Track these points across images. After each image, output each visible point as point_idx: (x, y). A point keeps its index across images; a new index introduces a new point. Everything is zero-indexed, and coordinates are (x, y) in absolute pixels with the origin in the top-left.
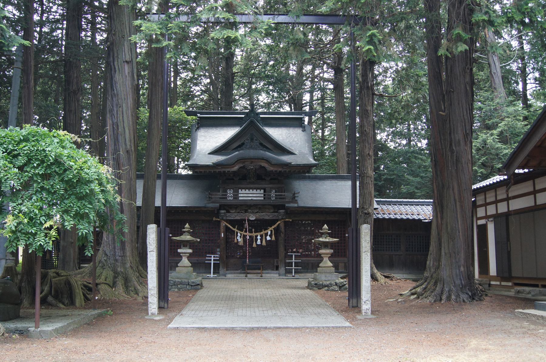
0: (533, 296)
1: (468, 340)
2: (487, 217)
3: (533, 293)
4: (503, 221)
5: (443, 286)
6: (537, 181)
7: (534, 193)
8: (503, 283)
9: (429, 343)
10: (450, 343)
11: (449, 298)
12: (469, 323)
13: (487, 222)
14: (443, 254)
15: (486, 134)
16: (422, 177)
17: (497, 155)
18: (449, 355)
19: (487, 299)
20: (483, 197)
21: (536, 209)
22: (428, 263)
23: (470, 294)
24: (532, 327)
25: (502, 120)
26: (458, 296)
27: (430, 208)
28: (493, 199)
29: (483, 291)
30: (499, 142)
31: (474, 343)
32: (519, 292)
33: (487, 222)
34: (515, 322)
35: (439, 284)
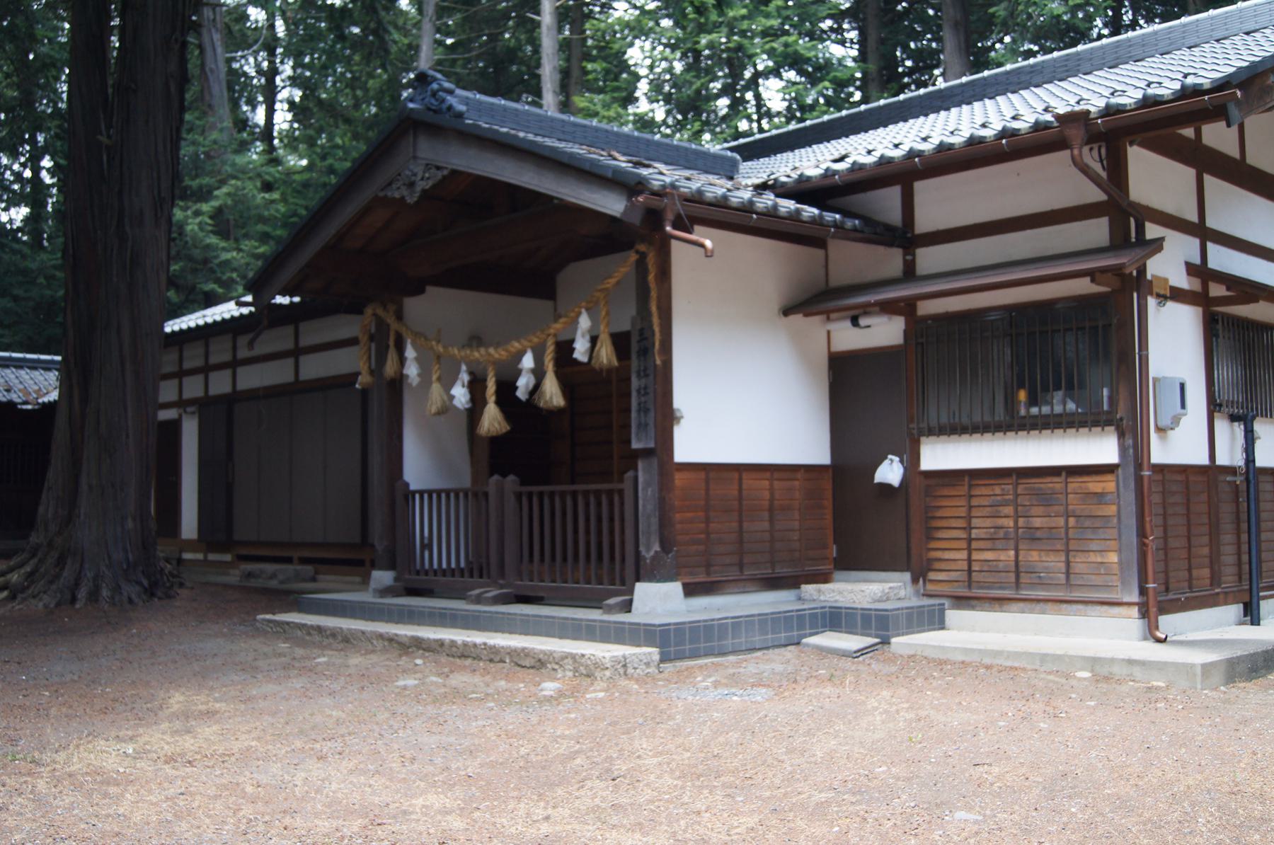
0: (282, 582)
1: (162, 694)
2: (181, 404)
3: (281, 577)
4: (220, 414)
5: (82, 565)
6: (304, 326)
7: (297, 353)
8: (211, 557)
9: (64, 710)
10: (117, 705)
11: (94, 596)
12: (154, 652)
13: (180, 416)
14: (84, 487)
15: (185, 209)
16: (16, 299)
17: (206, 261)
18: (121, 734)
19: (184, 592)
20: (201, 351)
21: (298, 389)
22: (41, 510)
23: (145, 583)
24: (299, 652)
25: (223, 182)
26: (117, 589)
27: (53, 376)
28: (199, 362)
29: (174, 576)
30: (212, 232)
31: (177, 700)
32: (250, 575)
33: (180, 416)
34: (256, 643)
35: (69, 561)
